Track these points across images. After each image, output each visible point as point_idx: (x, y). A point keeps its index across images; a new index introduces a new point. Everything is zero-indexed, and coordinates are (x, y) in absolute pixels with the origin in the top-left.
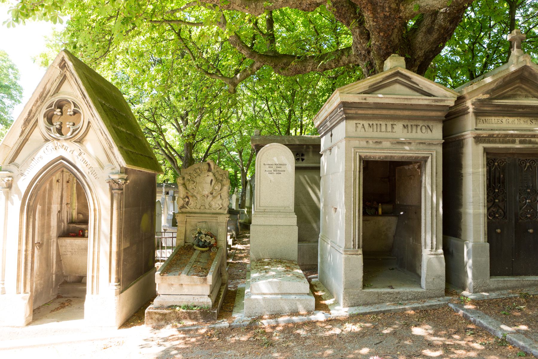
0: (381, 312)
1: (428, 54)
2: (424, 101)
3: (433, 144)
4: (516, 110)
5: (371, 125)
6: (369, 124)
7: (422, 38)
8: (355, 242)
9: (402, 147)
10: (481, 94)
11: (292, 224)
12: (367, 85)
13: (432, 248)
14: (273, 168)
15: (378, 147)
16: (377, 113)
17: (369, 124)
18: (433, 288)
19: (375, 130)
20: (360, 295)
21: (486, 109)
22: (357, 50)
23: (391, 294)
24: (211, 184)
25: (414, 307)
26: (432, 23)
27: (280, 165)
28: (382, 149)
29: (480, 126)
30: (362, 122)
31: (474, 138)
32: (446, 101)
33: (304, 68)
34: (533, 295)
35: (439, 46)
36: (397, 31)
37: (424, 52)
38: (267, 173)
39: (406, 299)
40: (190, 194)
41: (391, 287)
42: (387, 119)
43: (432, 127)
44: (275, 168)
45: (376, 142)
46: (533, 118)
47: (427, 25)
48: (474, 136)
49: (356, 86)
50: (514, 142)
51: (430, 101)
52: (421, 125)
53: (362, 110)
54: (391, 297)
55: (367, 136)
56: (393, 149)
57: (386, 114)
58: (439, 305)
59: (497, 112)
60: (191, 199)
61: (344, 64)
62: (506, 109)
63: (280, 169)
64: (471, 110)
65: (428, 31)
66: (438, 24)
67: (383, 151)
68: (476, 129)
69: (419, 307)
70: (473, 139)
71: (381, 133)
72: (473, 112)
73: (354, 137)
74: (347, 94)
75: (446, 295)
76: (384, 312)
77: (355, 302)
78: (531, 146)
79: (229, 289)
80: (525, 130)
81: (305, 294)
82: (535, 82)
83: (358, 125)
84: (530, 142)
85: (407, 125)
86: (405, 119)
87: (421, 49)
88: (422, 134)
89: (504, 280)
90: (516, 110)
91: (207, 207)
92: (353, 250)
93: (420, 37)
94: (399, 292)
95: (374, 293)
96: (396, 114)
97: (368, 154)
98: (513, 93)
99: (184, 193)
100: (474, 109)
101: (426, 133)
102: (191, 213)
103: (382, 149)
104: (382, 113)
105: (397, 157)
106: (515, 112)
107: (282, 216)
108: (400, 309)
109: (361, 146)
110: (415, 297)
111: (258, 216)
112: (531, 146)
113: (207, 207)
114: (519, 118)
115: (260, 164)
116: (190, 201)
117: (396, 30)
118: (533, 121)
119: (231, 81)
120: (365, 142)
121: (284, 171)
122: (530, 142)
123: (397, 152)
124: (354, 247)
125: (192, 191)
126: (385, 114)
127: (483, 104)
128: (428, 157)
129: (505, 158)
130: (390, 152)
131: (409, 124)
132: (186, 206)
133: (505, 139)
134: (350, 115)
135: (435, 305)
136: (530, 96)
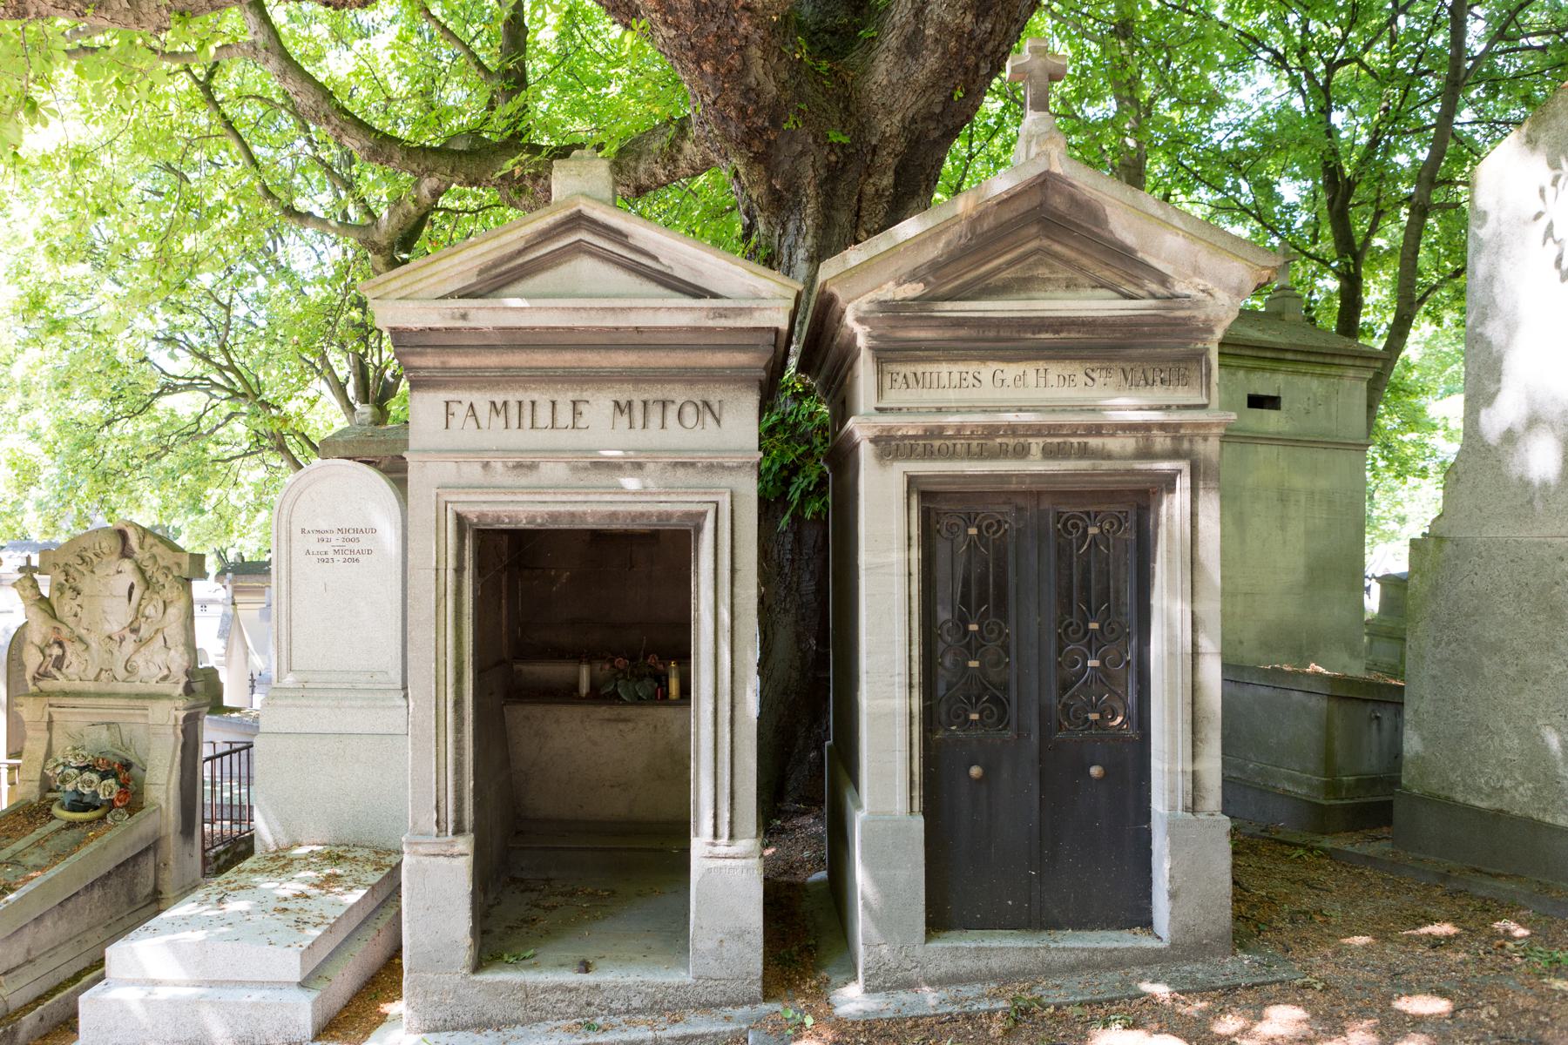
1: (919, 126)
2: (676, 313)
3: (722, 467)
4: (1029, 335)
5: (499, 406)
6: (493, 403)
7: (889, 73)
8: (442, 811)
9: (610, 483)
10: (891, 283)
11: (391, 731)
12: (470, 265)
13: (716, 835)
14: (334, 542)
15: (524, 481)
17: (493, 403)
18: (718, 974)
19: (514, 422)
20: (461, 992)
21: (915, 334)
23: (570, 991)
24: (130, 600)
26: (916, 15)
27: (356, 531)
29: (893, 398)
30: (466, 396)
31: (875, 441)
32: (757, 314)
34: (1058, 1008)
35: (956, 98)
36: (759, 53)
37: (903, 120)
38: (314, 558)
39: (623, 1008)
40: (65, 632)
41: (585, 967)
42: (556, 382)
45: (519, 466)
46: (1096, 365)
47: (903, 27)
48: (871, 433)
49: (427, 271)
50: (1022, 452)
51: (696, 314)
52: (679, 402)
53: (459, 355)
54: (570, 1002)
55: (486, 445)
56: (577, 489)
58: (715, 1035)
59: (959, 345)
60: (69, 648)
61: (692, 168)
62: (992, 334)
63: (355, 546)
64: (861, 342)
65: (908, 46)
66: (932, 19)
67: (538, 498)
68: (880, 410)
71: (533, 431)
73: (440, 451)
74: (397, 302)
75: (767, 996)
78: (1083, 465)
80: (1064, 410)
81: (288, 983)
82: (1096, 230)
83: (454, 407)
84: (1084, 452)
85: (630, 403)
86: (622, 381)
88: (685, 431)
89: (979, 949)
90: (1029, 335)
91: (120, 673)
92: (434, 839)
93: (883, 67)
94: (598, 986)
95: (513, 989)
96: (586, 364)
97: (485, 508)
98: (1019, 275)
99: (43, 630)
100: (869, 335)
101: (699, 426)
102: (66, 694)
104: (534, 364)
105: (594, 514)
106: (1029, 344)
107: (359, 703)
109: (463, 482)
110: (656, 1002)
111: (279, 702)
112: (1083, 465)
113: (120, 673)
114: (1041, 365)
115: (290, 532)
116: (68, 654)
117: (755, 52)
118: (1094, 375)
119: (363, 237)
120: (478, 468)
121: (369, 552)
122: (1084, 452)
124: (440, 831)
125: (71, 621)
126: (545, 364)
128: (703, 515)
129: (1005, 508)
130: (564, 498)
132: (54, 671)
133: (990, 443)
134: (422, 373)
136: (1086, 282)
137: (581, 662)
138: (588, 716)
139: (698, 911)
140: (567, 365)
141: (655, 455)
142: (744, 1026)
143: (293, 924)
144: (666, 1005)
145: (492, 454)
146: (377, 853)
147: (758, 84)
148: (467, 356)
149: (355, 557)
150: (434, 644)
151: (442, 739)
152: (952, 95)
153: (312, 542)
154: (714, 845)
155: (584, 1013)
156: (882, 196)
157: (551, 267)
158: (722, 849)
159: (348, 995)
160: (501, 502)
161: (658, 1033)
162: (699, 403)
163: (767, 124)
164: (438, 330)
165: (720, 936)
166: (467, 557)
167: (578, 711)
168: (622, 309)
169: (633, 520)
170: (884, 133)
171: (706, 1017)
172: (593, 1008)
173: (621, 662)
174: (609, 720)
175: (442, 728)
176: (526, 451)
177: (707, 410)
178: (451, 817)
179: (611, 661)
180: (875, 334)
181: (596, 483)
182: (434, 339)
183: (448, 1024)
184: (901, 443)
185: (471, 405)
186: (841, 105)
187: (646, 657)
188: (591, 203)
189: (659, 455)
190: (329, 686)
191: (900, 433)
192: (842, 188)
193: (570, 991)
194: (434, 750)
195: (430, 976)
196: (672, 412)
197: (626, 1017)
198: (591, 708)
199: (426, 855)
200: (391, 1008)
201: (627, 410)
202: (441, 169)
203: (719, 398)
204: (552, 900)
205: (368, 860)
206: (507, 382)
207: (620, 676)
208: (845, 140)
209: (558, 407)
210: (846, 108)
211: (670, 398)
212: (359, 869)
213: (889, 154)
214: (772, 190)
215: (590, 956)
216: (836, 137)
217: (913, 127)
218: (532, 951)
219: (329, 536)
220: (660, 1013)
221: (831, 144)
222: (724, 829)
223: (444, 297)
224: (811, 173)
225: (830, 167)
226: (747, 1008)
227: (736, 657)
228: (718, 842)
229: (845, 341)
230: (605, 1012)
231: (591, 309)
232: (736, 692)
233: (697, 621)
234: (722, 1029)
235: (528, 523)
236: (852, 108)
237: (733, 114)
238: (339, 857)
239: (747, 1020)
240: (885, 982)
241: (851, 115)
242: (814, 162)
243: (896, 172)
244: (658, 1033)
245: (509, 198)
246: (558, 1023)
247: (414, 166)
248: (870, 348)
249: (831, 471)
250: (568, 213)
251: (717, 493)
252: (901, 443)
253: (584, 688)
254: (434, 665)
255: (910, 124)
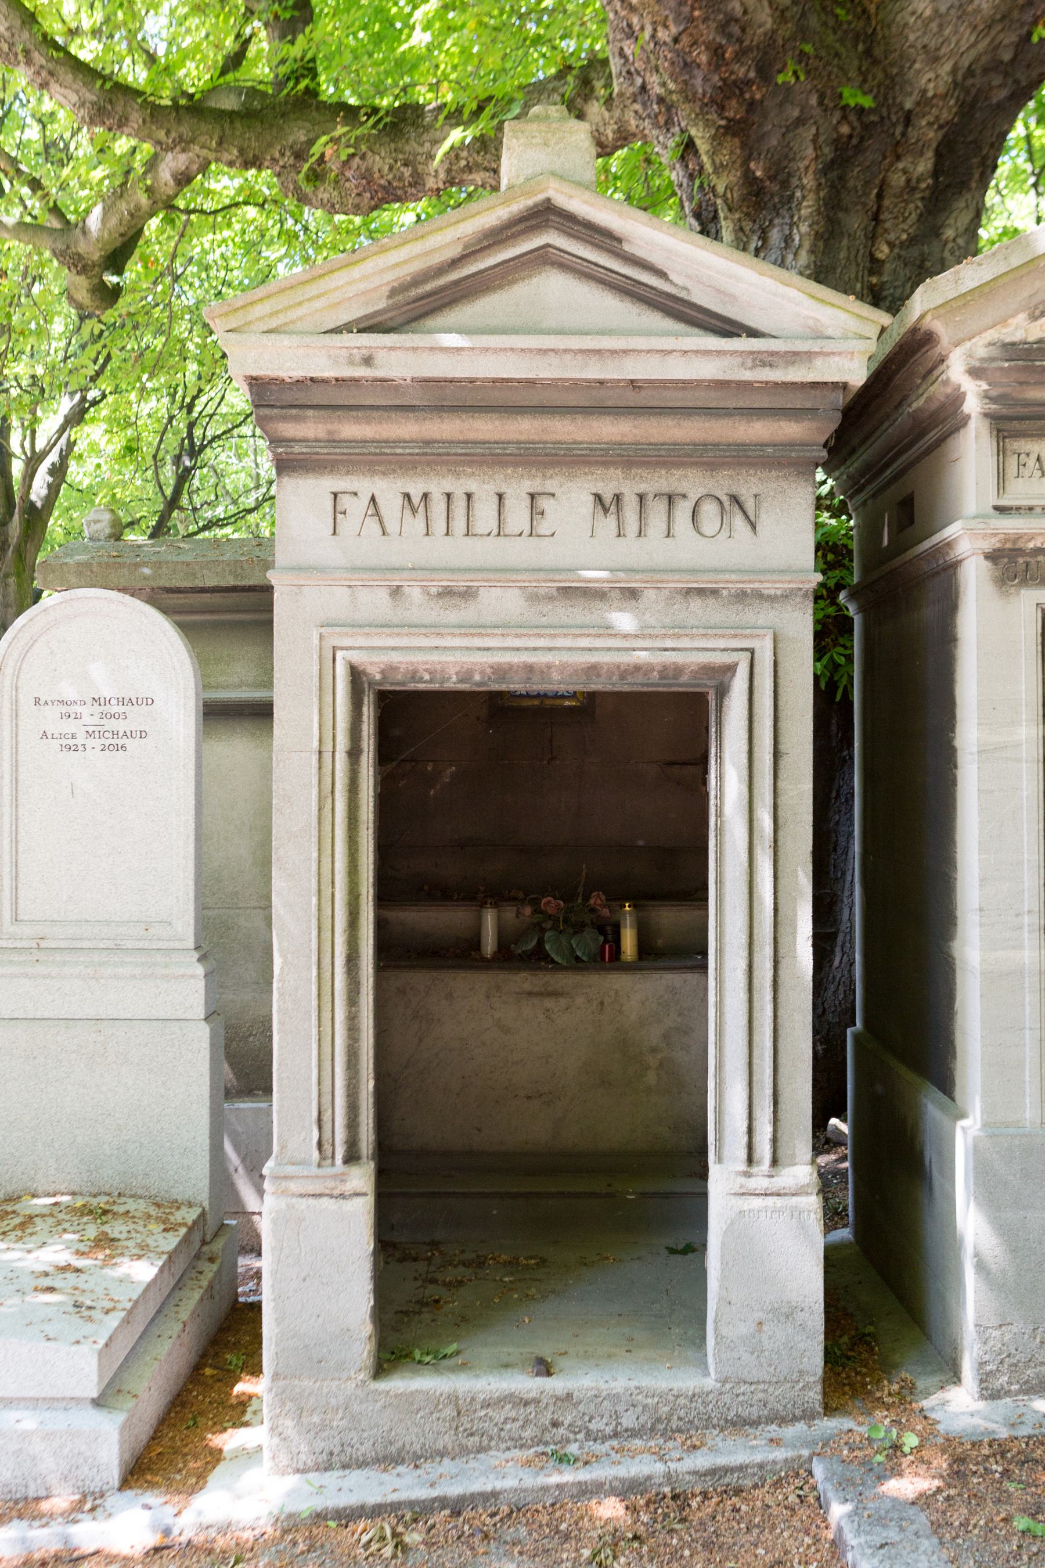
0: (443, 1502)
3: (759, 595)
5: (416, 500)
6: (407, 496)
8: (327, 1127)
10: (1022, 317)
11: (180, 1014)
12: (377, 281)
13: (750, 1160)
14: (87, 719)
16: (446, 436)
17: (407, 496)
18: (755, 1374)
19: (439, 525)
20: (356, 1408)
22: (629, 72)
23: (526, 1404)
25: (622, 1481)
27: (121, 701)
28: (479, 628)
29: (1020, 492)
30: (366, 485)
31: (993, 556)
32: (818, 362)
33: (407, 172)
37: (954, 71)
38: (56, 744)
39: (608, 1430)
41: (544, 1368)
43: (757, 506)
44: (96, 720)
45: (447, 593)
48: (989, 545)
52: (693, 497)
53: (357, 421)
54: (527, 1421)
55: (396, 561)
56: (537, 629)
57: (496, 437)
58: (761, 1466)
63: (121, 726)
64: (973, 405)
67: (478, 642)
68: (1000, 510)
69: (649, 1478)
70: (987, 565)
72: (986, 415)
75: (829, 1410)
76: (456, 1507)
77: (335, 1446)
79: (241, 1299)
81: (83, 1399)
83: (345, 501)
85: (618, 498)
86: (606, 464)
87: (934, 59)
92: (314, 1170)
94: (569, 1396)
95: (436, 1402)
97: (395, 658)
100: (986, 396)
101: (724, 534)
103: (479, 628)
104: (471, 436)
105: (563, 666)
108: (545, 1489)
110: (659, 1420)
119: (60, 246)
120: (383, 594)
121: (143, 734)
123: (560, 642)
124: (323, 1158)
126: (488, 437)
127: (1033, 370)
128: (731, 669)
130: (518, 643)
131: (629, 492)
134: (297, 449)
135: (741, 1468)
137: (483, 905)
138: (498, 988)
139: (723, 1278)
140: (523, 438)
141: (658, 577)
142: (805, 1453)
143: (72, 1310)
144: (675, 1423)
145: (406, 575)
146: (158, 1205)
147: (745, 12)
148: (368, 423)
149: (120, 742)
150: (314, 868)
151: (327, 1015)
152: (1030, 34)
153: (51, 719)
154: (747, 1175)
155: (547, 1437)
156: (914, 189)
157: (500, 287)
158: (759, 1183)
159: (154, 1422)
160: (419, 649)
161: (673, 1466)
162: (725, 499)
163: (752, 74)
164: (324, 381)
165: (759, 1315)
166: (365, 734)
167: (482, 980)
168: (613, 352)
169: (622, 677)
170: (924, 91)
171: (740, 1440)
172: (561, 1430)
173: (551, 904)
174: (530, 994)
175: (327, 998)
176: (459, 570)
177: (736, 508)
178: (340, 1135)
179: (535, 902)
180: (994, 393)
181: (565, 620)
182: (318, 396)
183: (335, 1459)
184: (1032, 560)
185: (373, 499)
186: (861, 47)
187: (586, 898)
188: (567, 189)
189: (665, 577)
190: (79, 945)
191: (1031, 545)
192: (855, 177)
193: (526, 1404)
194: (314, 1031)
195: (307, 1383)
196: (683, 511)
197: (615, 1443)
198: (502, 976)
199: (302, 1196)
200: (231, 1440)
201: (613, 508)
202: (203, 139)
203: (755, 491)
204: (451, 1274)
205: (149, 1216)
206: (429, 464)
207: (548, 925)
208: (867, 102)
209: (508, 502)
210: (868, 52)
211: (680, 490)
212: (141, 1229)
213: (930, 124)
214: (749, 178)
215: (546, 1351)
216: (854, 97)
217: (969, 82)
218: (454, 1347)
219: (78, 709)
220: (668, 1435)
221: (845, 108)
222: (764, 1149)
223: (336, 331)
224: (810, 152)
225: (840, 144)
226: (800, 1426)
227: (780, 887)
228: (754, 1170)
229: (934, 406)
230: (581, 1436)
231: (565, 351)
232: (781, 941)
233: (720, 831)
234: (771, 1457)
235: (460, 681)
236: (878, 52)
237: (704, 58)
238: (105, 1212)
239: (806, 1444)
240: (1010, 1383)
241: (875, 62)
242: (817, 135)
243: (938, 154)
244: (673, 1466)
245: (297, 189)
246: (509, 1455)
247: (161, 134)
248: (986, 415)
249: (861, 610)
250: (530, 202)
251: (752, 636)
252: (1032, 560)
253: (489, 945)
254: (314, 900)
255: (965, 78)
